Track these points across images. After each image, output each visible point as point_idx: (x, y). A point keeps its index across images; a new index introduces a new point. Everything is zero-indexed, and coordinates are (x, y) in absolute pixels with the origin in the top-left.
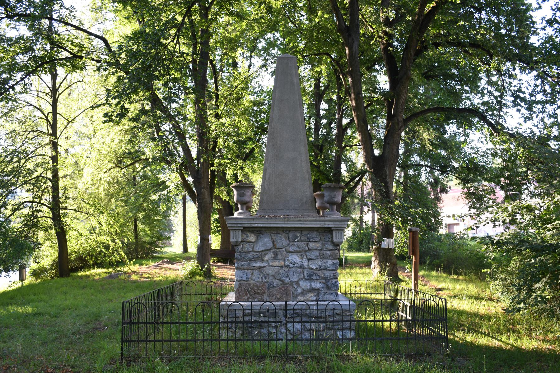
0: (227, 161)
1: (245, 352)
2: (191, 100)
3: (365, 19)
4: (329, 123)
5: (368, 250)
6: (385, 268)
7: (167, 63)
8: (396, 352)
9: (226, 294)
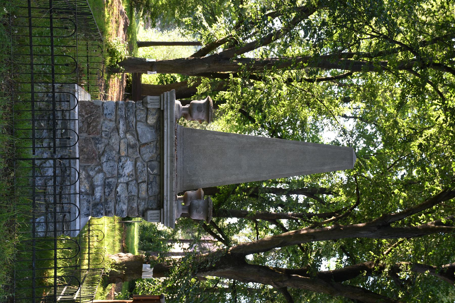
0: (239, 92)
1: (19, 112)
2: (307, 52)
3: (398, 245)
4: (282, 204)
5: (140, 249)
6: (119, 269)
7: (349, 24)
8: (18, 284)
9: (88, 90)
